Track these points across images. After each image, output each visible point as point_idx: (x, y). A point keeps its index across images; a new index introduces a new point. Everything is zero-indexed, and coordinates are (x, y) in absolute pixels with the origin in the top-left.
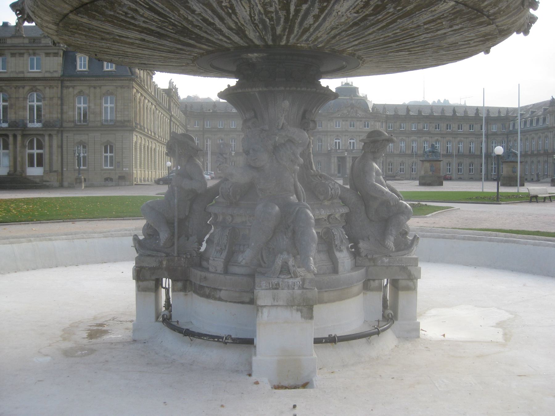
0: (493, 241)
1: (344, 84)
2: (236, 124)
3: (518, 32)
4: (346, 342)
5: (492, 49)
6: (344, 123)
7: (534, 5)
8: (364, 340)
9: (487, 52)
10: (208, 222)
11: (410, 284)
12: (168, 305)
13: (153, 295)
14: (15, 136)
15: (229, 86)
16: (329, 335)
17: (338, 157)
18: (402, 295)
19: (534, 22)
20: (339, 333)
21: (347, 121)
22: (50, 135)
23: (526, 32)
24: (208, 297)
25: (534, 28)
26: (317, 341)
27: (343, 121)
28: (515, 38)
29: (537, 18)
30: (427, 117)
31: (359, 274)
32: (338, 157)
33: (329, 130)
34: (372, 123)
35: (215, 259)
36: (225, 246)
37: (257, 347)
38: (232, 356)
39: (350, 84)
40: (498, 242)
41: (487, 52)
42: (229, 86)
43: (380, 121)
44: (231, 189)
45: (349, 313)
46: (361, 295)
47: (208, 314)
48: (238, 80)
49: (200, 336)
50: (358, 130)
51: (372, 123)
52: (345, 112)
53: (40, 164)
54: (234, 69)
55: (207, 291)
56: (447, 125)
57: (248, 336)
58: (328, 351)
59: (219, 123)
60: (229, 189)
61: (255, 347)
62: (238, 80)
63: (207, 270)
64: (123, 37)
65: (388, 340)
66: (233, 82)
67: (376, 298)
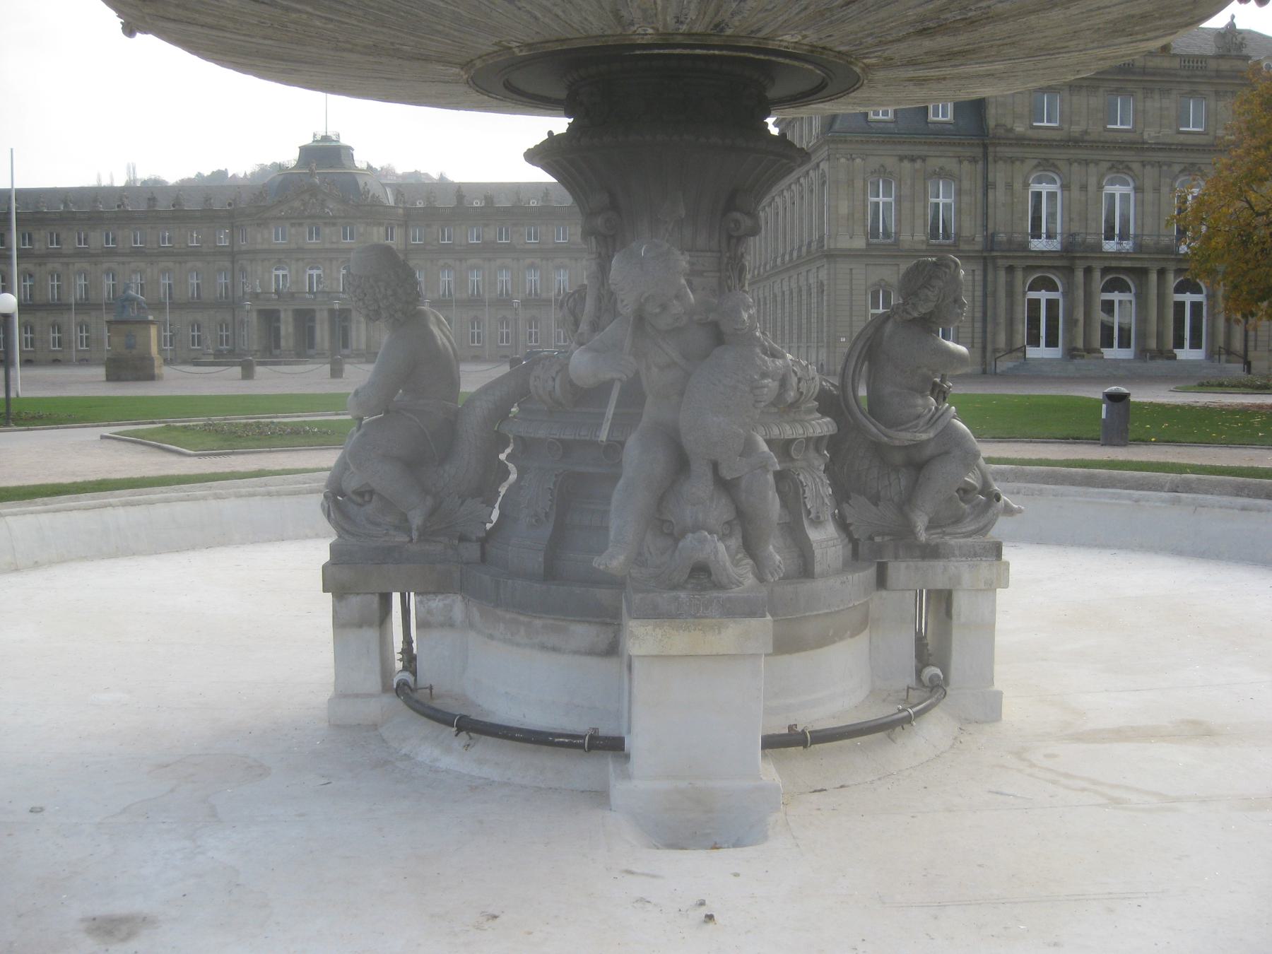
1: (319, 138)
2: (569, 233)
4: (436, 724)
6: (293, 231)
12: (410, 659)
13: (371, 634)
14: (1162, 273)
15: (550, 133)
16: (790, 728)
17: (260, 312)
21: (300, 225)
22: (1010, 269)
26: (772, 743)
27: (293, 225)
30: (506, 211)
32: (260, 312)
33: (259, 247)
34: (362, 230)
37: (633, 758)
38: (581, 769)
39: (334, 138)
42: (550, 133)
43: (380, 224)
45: (837, 681)
47: (519, 676)
48: (571, 120)
50: (328, 246)
51: (362, 230)
52: (297, 204)
53: (1124, 343)
54: (562, 94)
56: (52, 234)
57: (606, 729)
58: (803, 764)
59: (277, 234)
61: (627, 757)
62: (571, 120)
66: (560, 124)
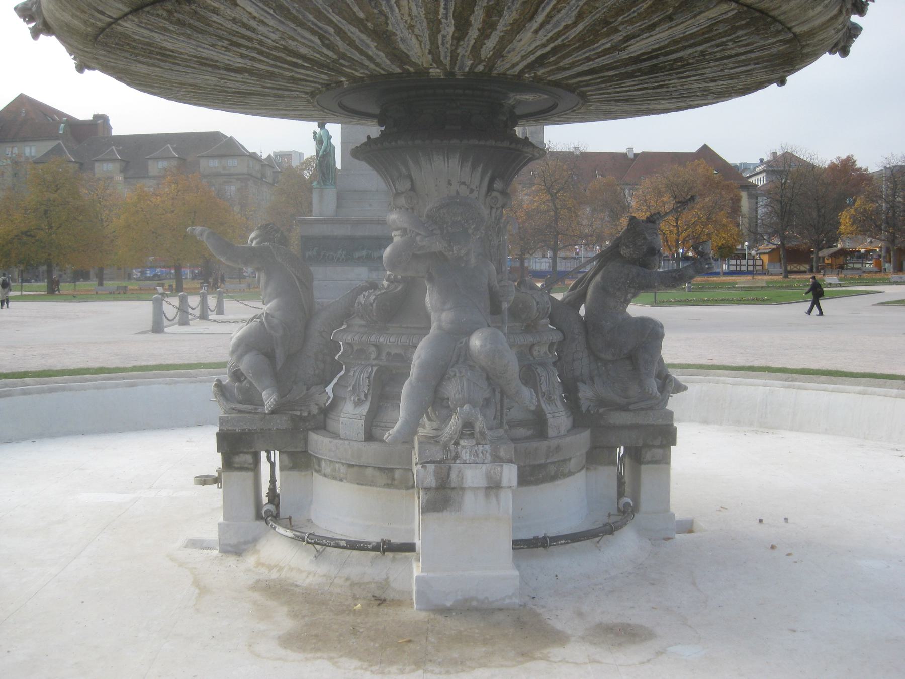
0: (30, 393)
3: (832, 52)
5: (790, 79)
7: (861, 9)
8: (587, 543)
9: (782, 82)
10: (336, 358)
11: (659, 452)
13: (250, 475)
15: (368, 137)
18: (647, 472)
19: (856, 36)
20: (553, 532)
23: (845, 52)
24: (553, 478)
25: (857, 46)
28: (827, 61)
29: (861, 29)
31: (583, 438)
35: (556, 415)
36: (366, 396)
40: (38, 393)
41: (782, 82)
44: (374, 305)
46: (584, 471)
49: (555, 540)
54: (377, 111)
55: (552, 469)
60: (371, 305)
63: (336, 435)
64: (643, 31)
65: (627, 543)
67: (606, 476)
